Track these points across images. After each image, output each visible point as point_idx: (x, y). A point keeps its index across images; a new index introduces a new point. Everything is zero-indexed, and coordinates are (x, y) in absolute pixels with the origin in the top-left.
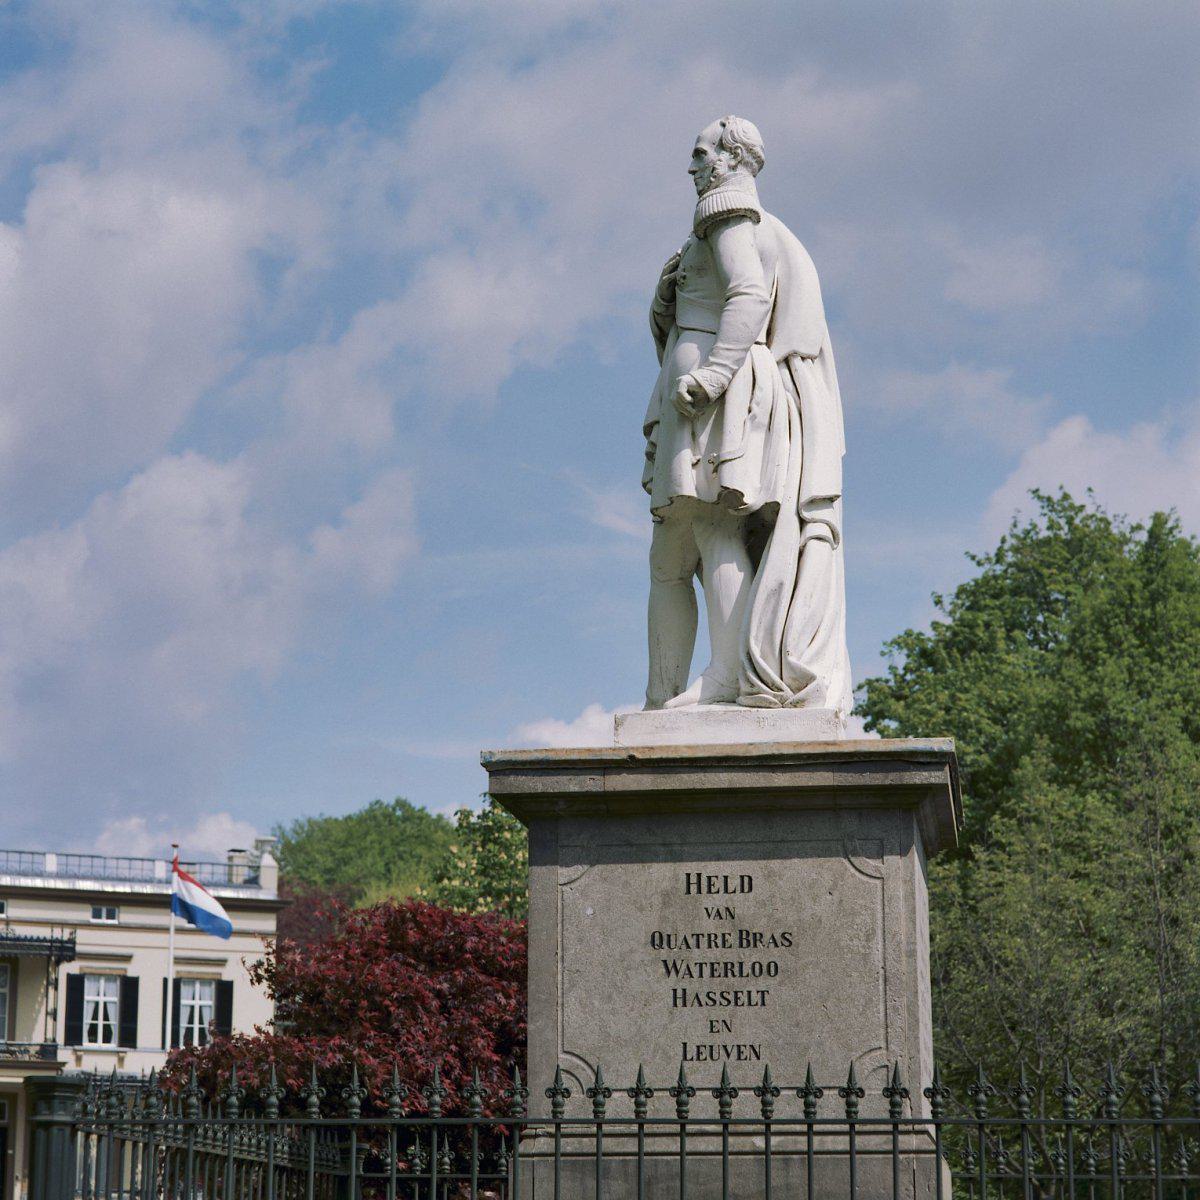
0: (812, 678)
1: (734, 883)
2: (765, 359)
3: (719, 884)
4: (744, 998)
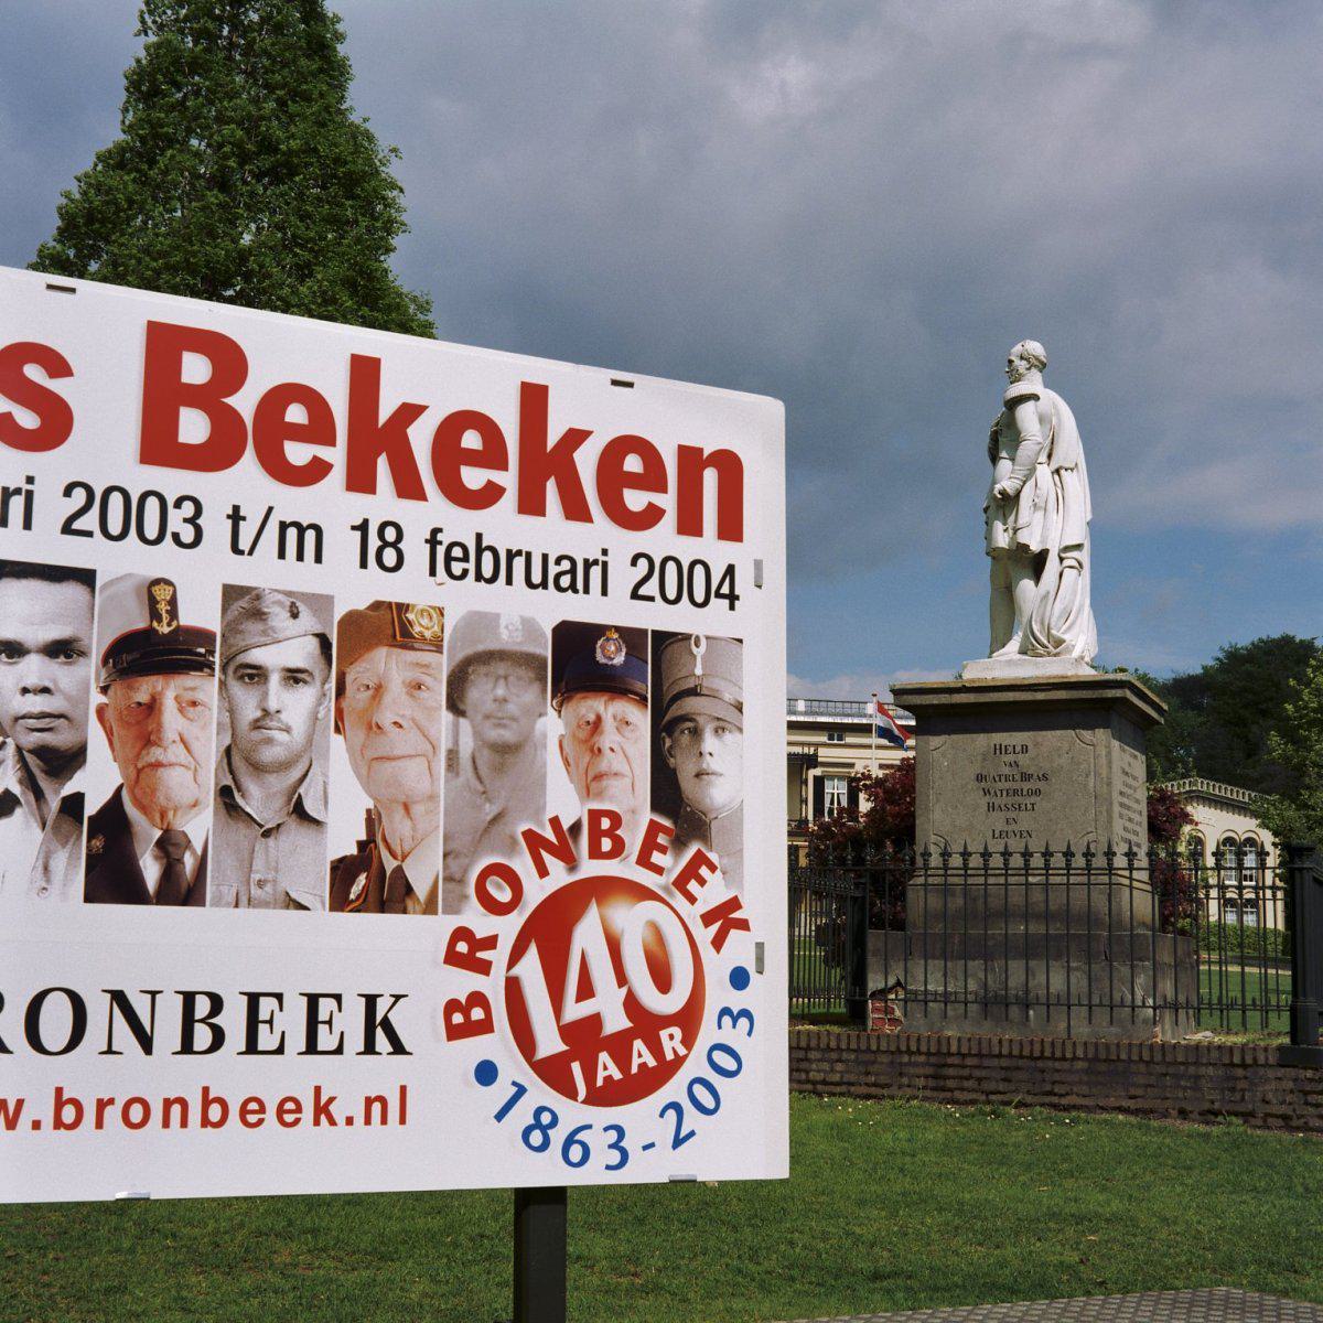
0: (1064, 641)
1: (1018, 749)
2: (1044, 472)
3: (1011, 749)
4: (1023, 807)
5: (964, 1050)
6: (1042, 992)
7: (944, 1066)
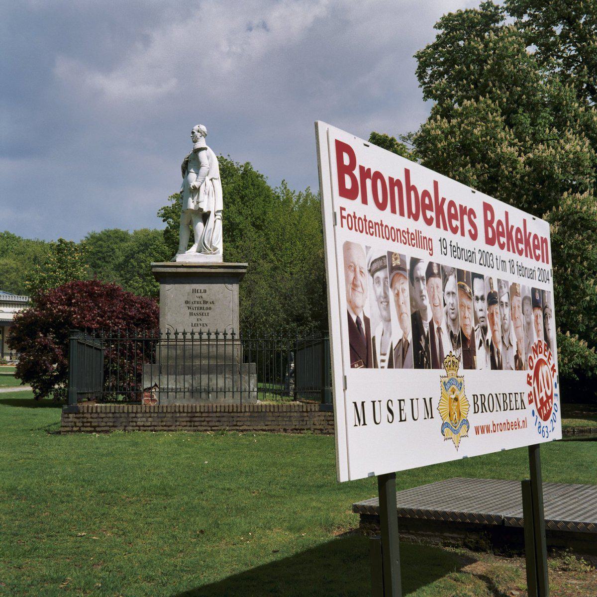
0: (217, 249)
1: (202, 291)
3: (199, 291)
4: (204, 314)
5: (202, 411)
6: (215, 387)
7: (194, 417)
